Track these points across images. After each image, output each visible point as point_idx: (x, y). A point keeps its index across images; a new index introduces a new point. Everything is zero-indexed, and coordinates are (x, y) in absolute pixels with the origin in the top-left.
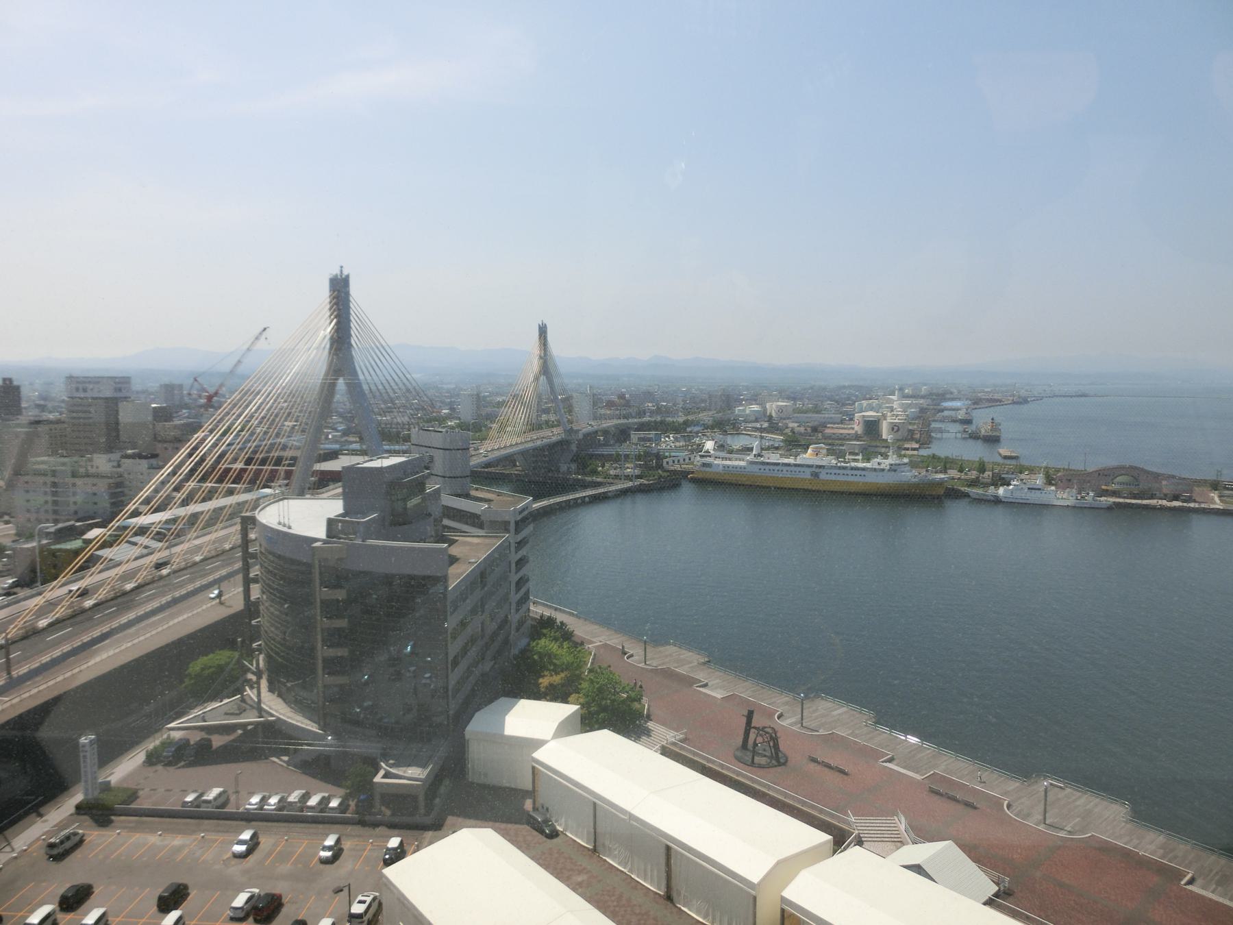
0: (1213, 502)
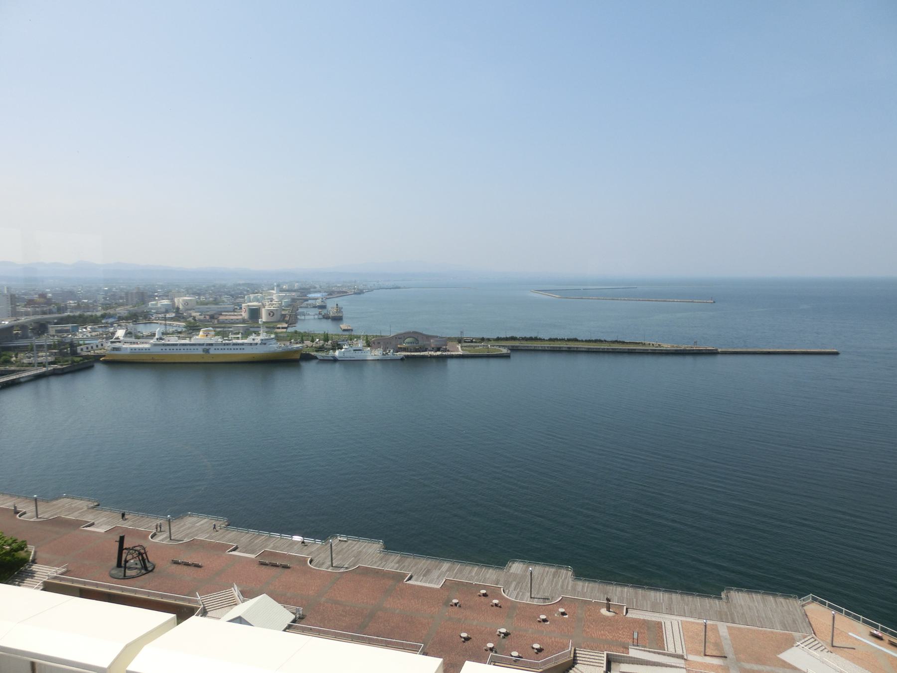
0: (458, 351)
